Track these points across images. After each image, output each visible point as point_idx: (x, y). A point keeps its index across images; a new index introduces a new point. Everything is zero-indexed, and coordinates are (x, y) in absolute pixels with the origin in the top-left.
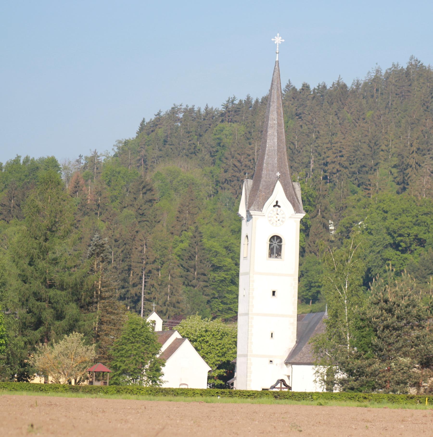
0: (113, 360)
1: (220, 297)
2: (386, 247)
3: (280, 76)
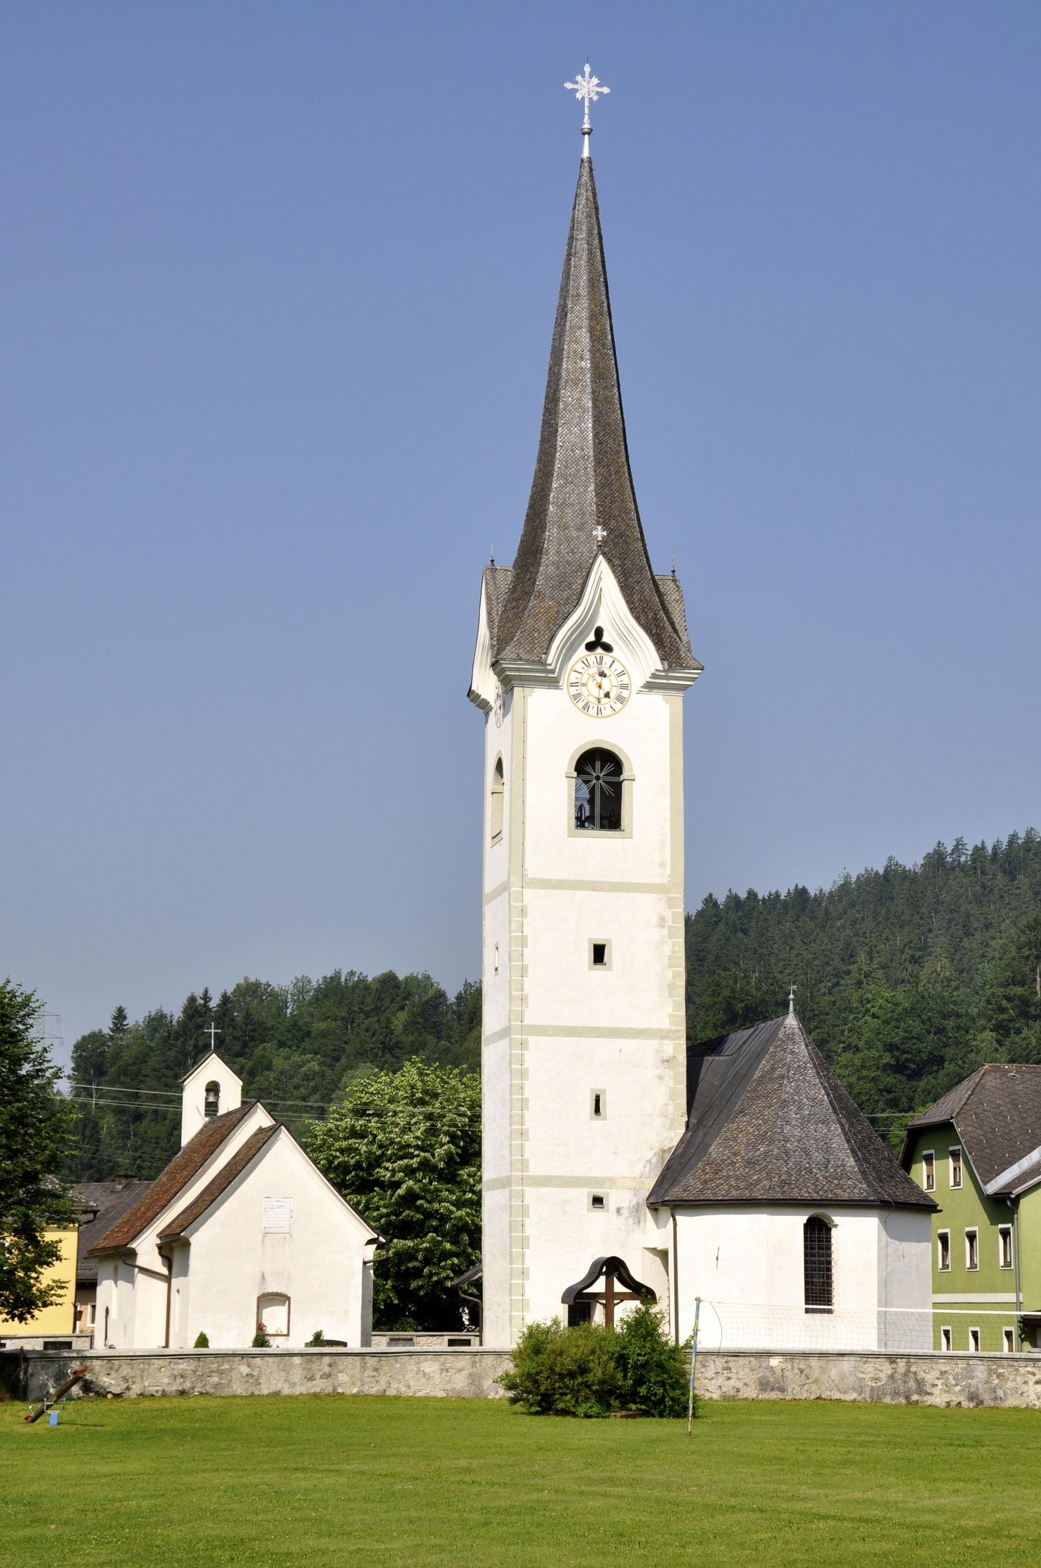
3: (597, 209)
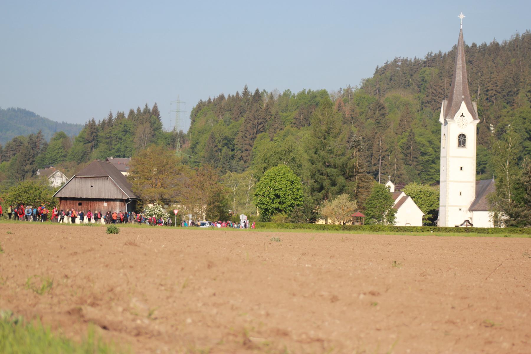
0: (366, 209)
1: (426, 171)
2: (525, 140)
